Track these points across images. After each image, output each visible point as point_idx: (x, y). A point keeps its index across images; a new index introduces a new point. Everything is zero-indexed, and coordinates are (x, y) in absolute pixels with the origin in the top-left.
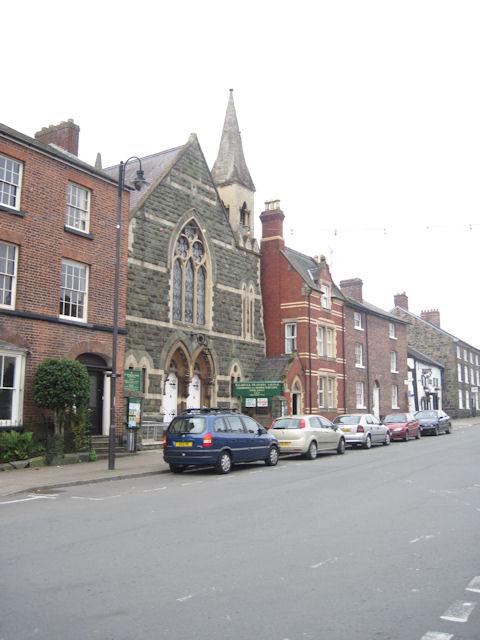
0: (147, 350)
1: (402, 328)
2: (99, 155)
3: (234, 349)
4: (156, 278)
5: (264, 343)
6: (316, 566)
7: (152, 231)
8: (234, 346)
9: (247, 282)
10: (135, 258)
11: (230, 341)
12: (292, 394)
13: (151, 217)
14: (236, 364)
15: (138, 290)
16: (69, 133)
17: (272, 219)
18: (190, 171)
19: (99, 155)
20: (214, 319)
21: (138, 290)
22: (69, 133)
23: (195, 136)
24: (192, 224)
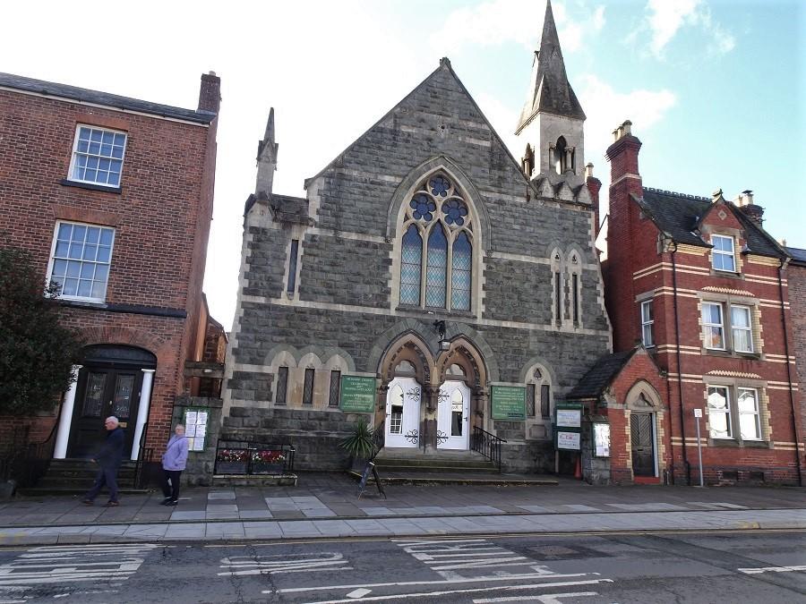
0: (342, 346)
1: (304, 426)
2: (272, 110)
3: (533, 343)
4: (362, 251)
5: (609, 334)
6: (608, 580)
7: (356, 191)
8: (533, 339)
9: (565, 246)
10: (321, 227)
11: (525, 333)
12: (627, 415)
13: (355, 173)
14: (538, 365)
15: (327, 268)
16: (260, 142)
17: (625, 150)
18: (434, 108)
19: (272, 110)
20: (485, 273)
21: (327, 268)
22: (260, 142)
23: (445, 62)
24: (441, 181)
